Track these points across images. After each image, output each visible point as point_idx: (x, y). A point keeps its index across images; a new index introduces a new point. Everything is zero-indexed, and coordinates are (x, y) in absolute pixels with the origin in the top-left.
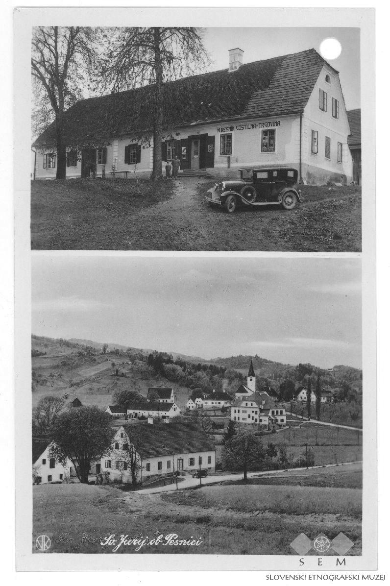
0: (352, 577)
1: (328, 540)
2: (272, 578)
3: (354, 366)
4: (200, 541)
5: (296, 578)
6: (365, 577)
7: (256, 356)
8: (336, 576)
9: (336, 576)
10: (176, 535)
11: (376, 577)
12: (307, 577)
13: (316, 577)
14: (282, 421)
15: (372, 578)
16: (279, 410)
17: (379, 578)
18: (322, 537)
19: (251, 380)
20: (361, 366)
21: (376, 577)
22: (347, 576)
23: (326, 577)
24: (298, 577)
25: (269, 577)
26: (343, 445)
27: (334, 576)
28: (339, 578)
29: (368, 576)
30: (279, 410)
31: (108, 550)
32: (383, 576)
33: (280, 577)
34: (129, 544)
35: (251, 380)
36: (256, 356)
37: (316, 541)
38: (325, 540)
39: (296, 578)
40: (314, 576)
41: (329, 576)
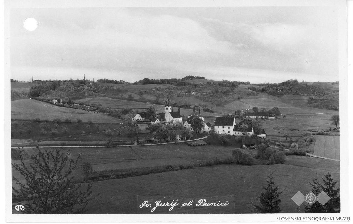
0: (329, 218)
1: (315, 196)
2: (280, 219)
4: (227, 203)
5: (295, 219)
6: (338, 218)
8: (320, 218)
9: (320, 218)
10: (141, 207)
11: (344, 218)
12: (302, 219)
13: (307, 218)
15: (342, 219)
17: (346, 219)
18: (311, 194)
21: (344, 218)
23: (313, 219)
24: (296, 218)
25: (278, 218)
27: (318, 218)
28: (321, 219)
29: (339, 218)
31: (146, 211)
33: (285, 219)
37: (308, 196)
39: (295, 219)
40: (306, 218)
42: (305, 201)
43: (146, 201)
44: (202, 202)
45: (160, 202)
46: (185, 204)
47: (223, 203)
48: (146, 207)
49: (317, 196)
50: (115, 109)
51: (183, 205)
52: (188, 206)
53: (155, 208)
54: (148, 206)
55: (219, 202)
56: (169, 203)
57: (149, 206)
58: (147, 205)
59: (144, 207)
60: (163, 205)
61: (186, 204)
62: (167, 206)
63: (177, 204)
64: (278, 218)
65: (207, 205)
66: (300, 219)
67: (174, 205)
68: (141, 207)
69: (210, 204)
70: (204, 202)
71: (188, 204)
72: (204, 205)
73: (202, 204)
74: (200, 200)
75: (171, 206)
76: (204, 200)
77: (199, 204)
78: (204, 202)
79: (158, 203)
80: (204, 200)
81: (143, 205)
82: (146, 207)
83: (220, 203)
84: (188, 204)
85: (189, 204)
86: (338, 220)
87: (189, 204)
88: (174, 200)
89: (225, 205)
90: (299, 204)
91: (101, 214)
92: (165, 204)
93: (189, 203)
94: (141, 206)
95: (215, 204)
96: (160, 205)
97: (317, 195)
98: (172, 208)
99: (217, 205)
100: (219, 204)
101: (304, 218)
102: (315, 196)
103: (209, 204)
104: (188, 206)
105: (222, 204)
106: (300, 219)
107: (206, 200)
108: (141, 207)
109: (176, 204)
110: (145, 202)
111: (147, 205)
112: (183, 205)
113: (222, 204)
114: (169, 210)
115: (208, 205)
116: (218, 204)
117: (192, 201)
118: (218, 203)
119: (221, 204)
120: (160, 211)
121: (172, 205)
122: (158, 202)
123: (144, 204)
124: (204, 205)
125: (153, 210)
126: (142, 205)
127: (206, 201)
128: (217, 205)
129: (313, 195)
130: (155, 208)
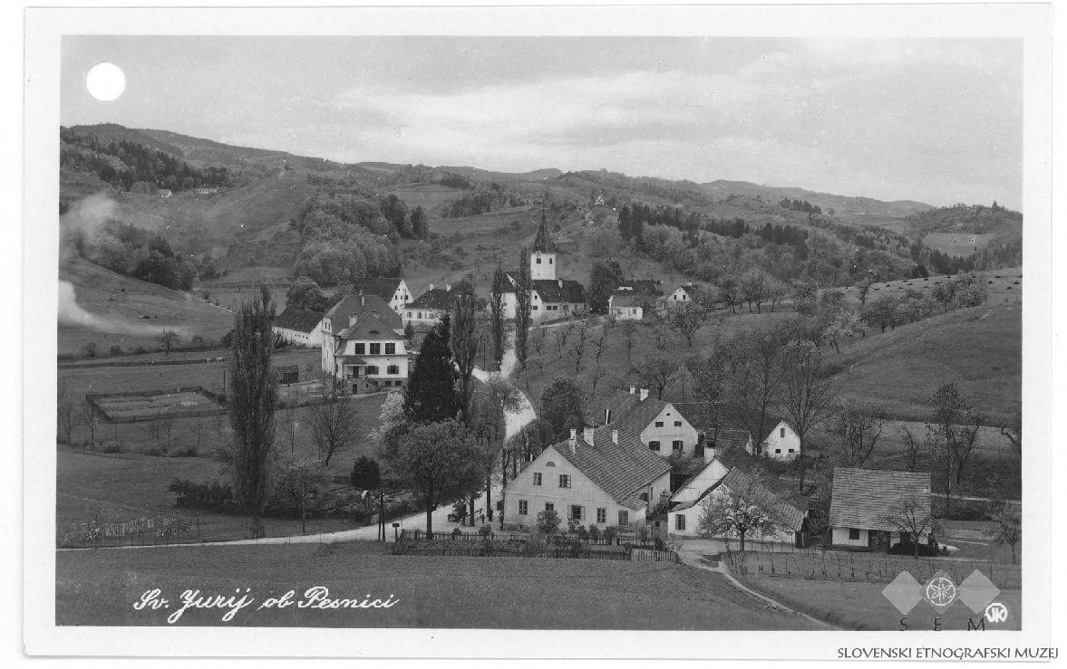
0: (996, 652)
1: (952, 585)
2: (849, 654)
3: (63, 283)
4: (392, 600)
5: (893, 655)
6: (1022, 651)
7: (995, 204)
8: (968, 651)
9: (968, 651)
10: (140, 608)
11: (1041, 652)
12: (914, 653)
13: (930, 652)
14: (393, 370)
15: (1034, 653)
16: (383, 344)
17: (1047, 654)
18: (941, 579)
19: (539, 261)
20: (60, 287)
21: (1041, 652)
22: (988, 651)
23: (948, 653)
24: (897, 652)
25: (843, 652)
26: (140, 451)
27: (964, 651)
28: (972, 654)
29: (1026, 651)
30: (383, 344)
31: (155, 618)
32: (1054, 651)
33: (863, 653)
34: (348, 600)
35: (539, 261)
36: (995, 204)
37: (931, 585)
38: (946, 584)
39: (893, 655)
40: (927, 650)
41: (953, 651)
42: (922, 601)
43: (154, 592)
44: (318, 596)
45: (195, 595)
46: (270, 602)
47: (380, 601)
48: (154, 608)
49: (961, 587)
50: (71, 363)
51: (266, 604)
52: (280, 606)
53: (180, 612)
54: (160, 605)
55: (368, 596)
56: (224, 598)
57: (164, 605)
58: (157, 601)
59: (148, 608)
60: (205, 604)
61: (275, 601)
62: (219, 605)
63: (246, 604)
64: (841, 651)
65: (332, 605)
66: (1007, 655)
67: (239, 604)
68: (138, 606)
69: (342, 603)
70: (320, 597)
71: (281, 602)
72: (320, 606)
73: (316, 602)
74: (310, 590)
75: (228, 609)
76: (320, 590)
77: (306, 601)
78: (320, 597)
79: (189, 598)
80: (320, 590)
81: (145, 602)
82: (154, 608)
83: (371, 600)
84: (281, 602)
85: (283, 601)
86: (1021, 656)
87: (283, 601)
88: (238, 590)
89: (385, 605)
90: (905, 609)
91: (507, 631)
92: (344, 604)
93: (284, 598)
94: (136, 604)
95: (356, 601)
96: (197, 603)
97: (958, 584)
98: (233, 612)
99: (363, 605)
100: (367, 604)
101: (920, 651)
102: (952, 585)
103: (337, 601)
104: (280, 606)
105: (378, 604)
106: (907, 653)
107: (327, 590)
108: (138, 606)
109: (246, 602)
110: (152, 594)
111: (157, 601)
112: (266, 604)
113: (378, 604)
114: (224, 619)
115: (335, 604)
116: (365, 602)
117: (293, 592)
118: (366, 598)
119: (374, 604)
120: (195, 618)
121: (230, 606)
122: (189, 595)
123: (148, 598)
124: (320, 606)
125: (172, 619)
126: (141, 602)
127: (327, 594)
128: (363, 605)
129: (946, 584)
130: (180, 612)
